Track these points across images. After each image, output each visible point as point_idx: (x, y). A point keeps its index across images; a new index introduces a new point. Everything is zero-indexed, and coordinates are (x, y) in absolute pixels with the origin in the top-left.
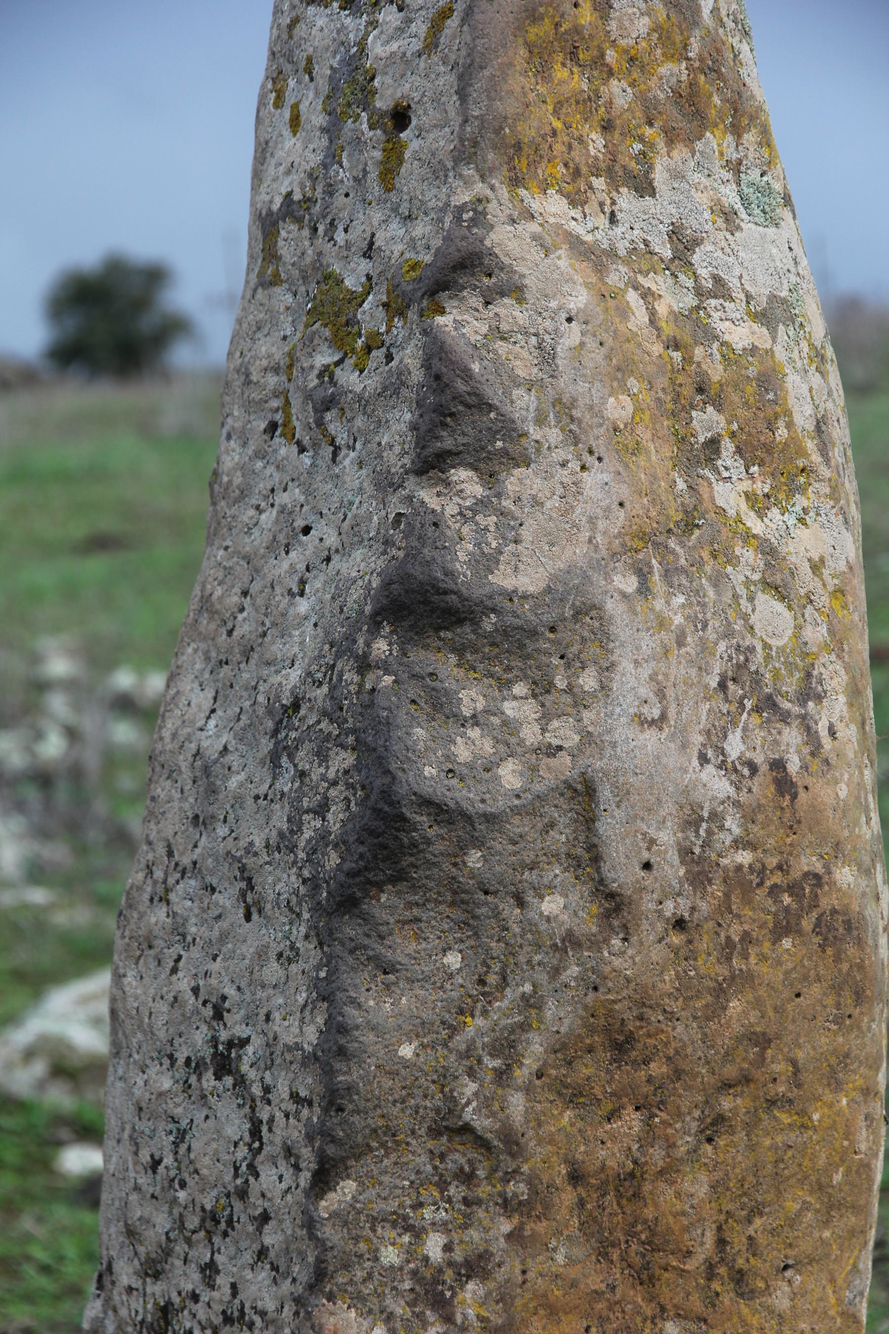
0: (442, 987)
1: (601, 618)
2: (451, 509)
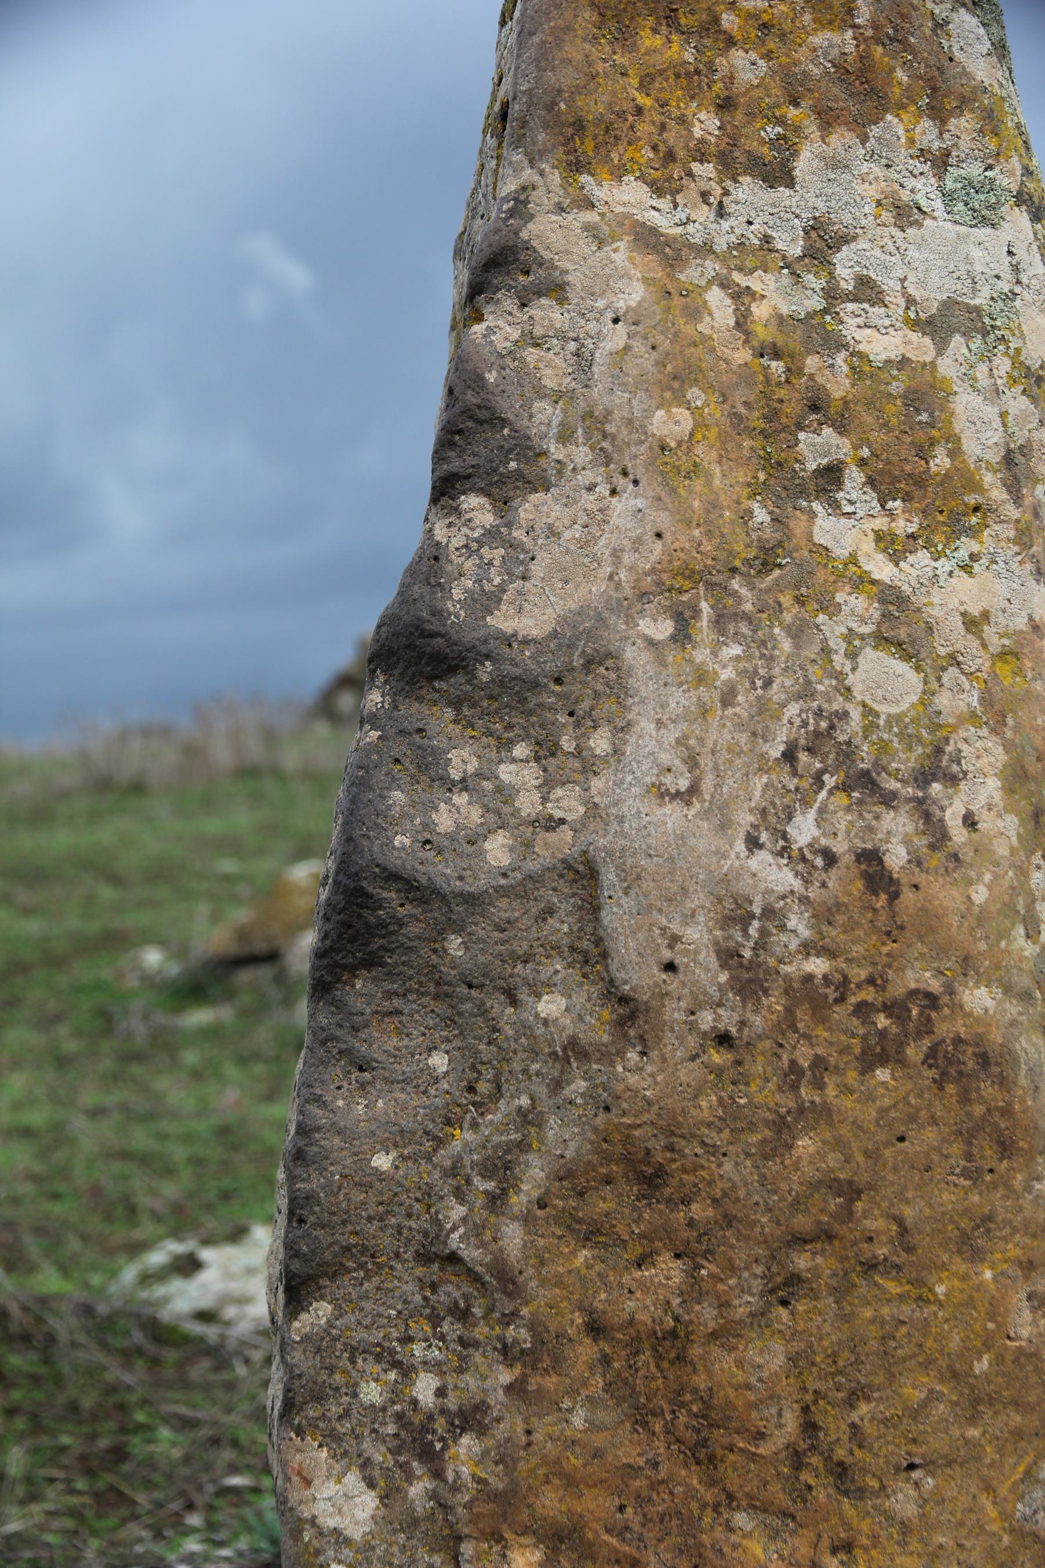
0: (425, 1092)
1: (618, 669)
2: (457, 541)
